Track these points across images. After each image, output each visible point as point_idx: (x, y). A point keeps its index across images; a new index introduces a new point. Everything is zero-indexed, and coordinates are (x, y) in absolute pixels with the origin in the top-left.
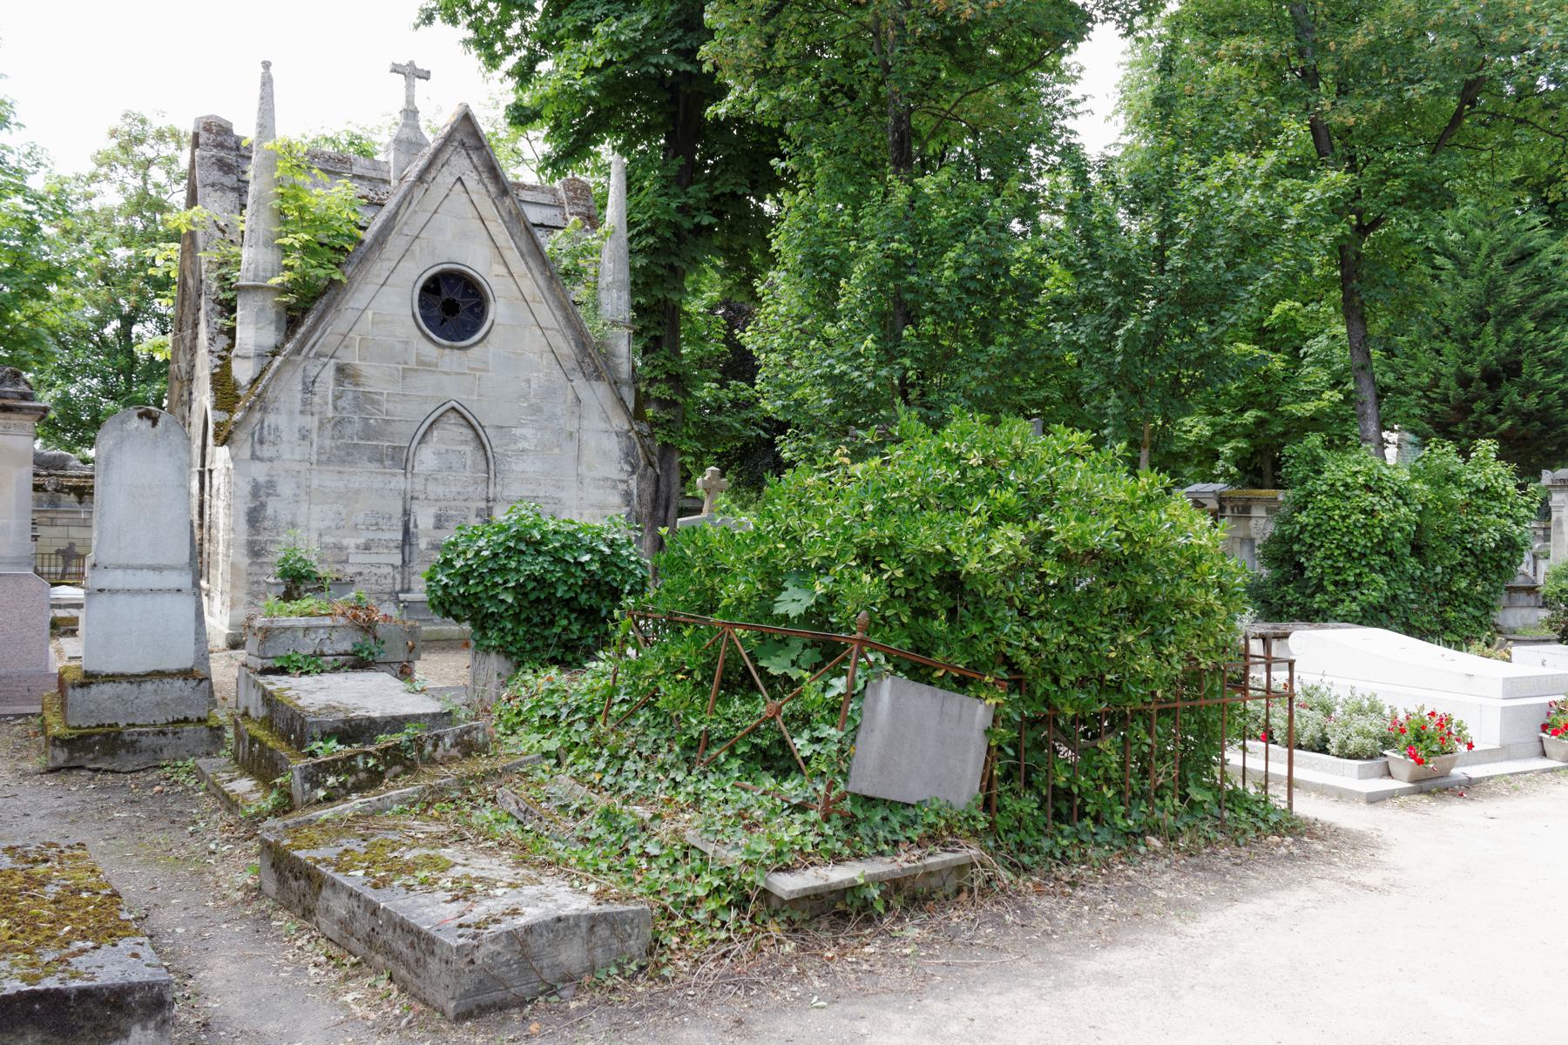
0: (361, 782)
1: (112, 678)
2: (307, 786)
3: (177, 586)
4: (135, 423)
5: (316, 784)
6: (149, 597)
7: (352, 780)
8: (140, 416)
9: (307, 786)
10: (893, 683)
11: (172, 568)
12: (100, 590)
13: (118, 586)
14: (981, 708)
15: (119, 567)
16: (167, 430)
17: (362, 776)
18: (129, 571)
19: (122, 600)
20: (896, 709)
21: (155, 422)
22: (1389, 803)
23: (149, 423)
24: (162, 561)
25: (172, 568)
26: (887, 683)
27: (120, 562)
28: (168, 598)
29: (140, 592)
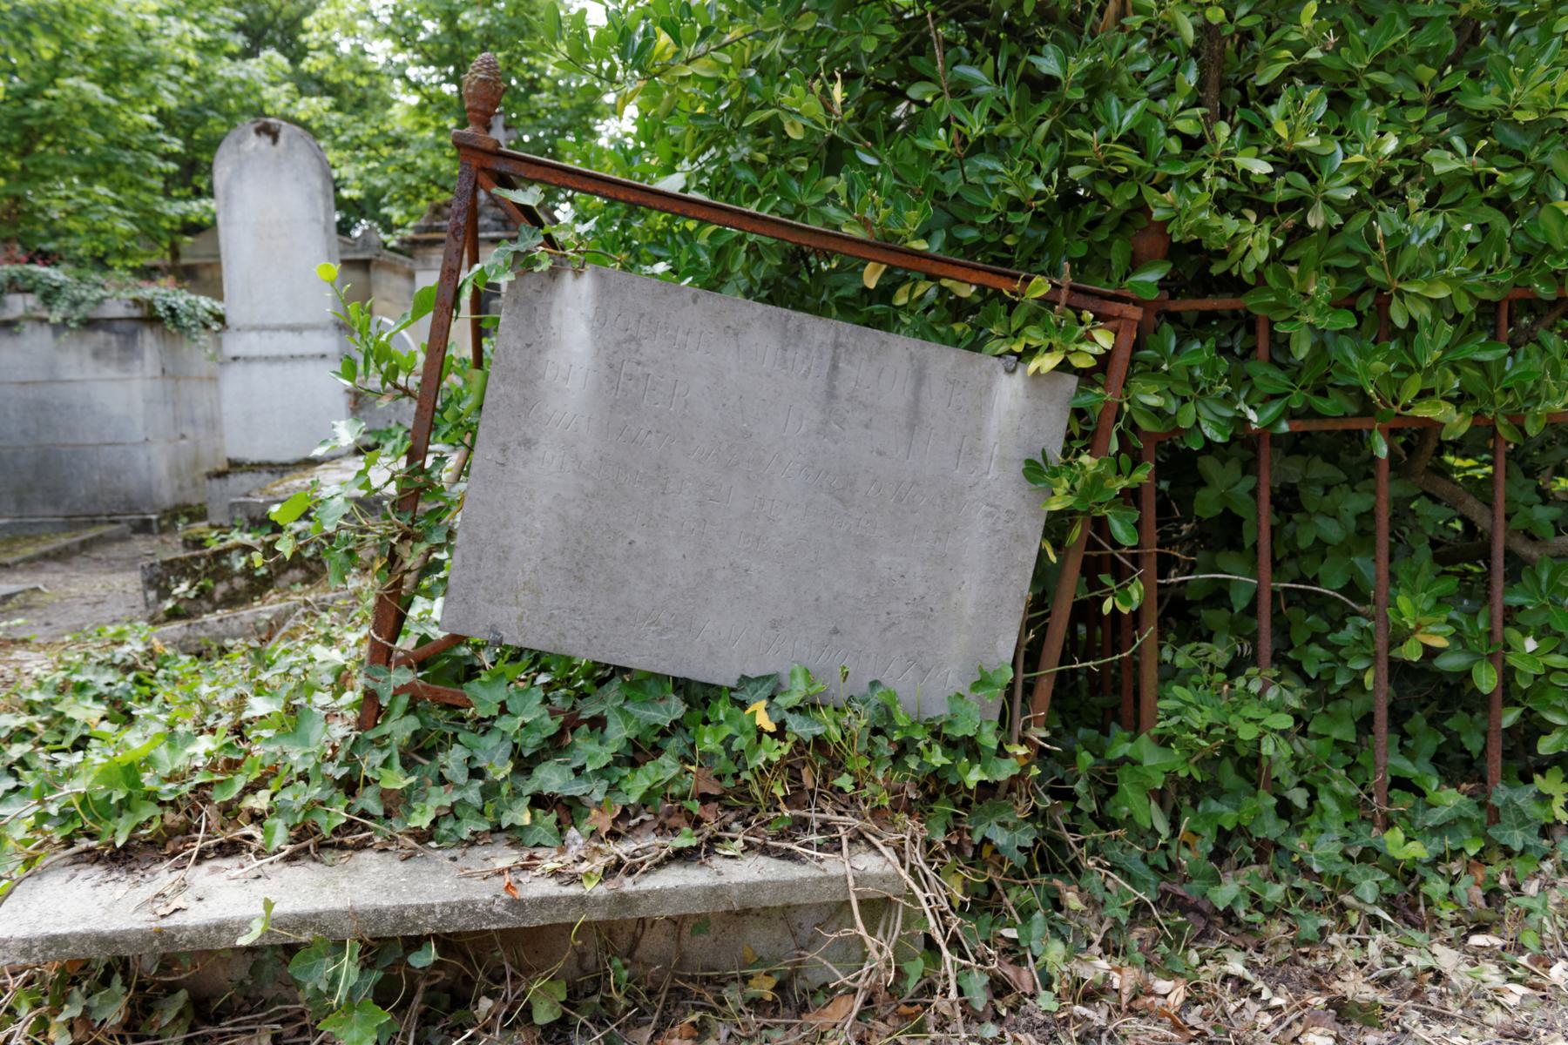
0: (235, 592)
1: (256, 467)
2: (152, 595)
3: (318, 350)
4: (255, 143)
5: (165, 593)
6: (289, 366)
7: (222, 588)
8: (258, 131)
9: (152, 595)
10: (604, 290)
11: (313, 328)
12: (235, 359)
13: (255, 352)
14: (1009, 393)
15: (254, 328)
16: (290, 147)
17: (240, 583)
18: (265, 334)
19: (258, 369)
20: (619, 377)
21: (275, 136)
22: (77, 560)
23: (268, 140)
24: (301, 318)
25: (313, 328)
26: (577, 297)
27: (255, 322)
28: (311, 367)
29: (279, 359)
